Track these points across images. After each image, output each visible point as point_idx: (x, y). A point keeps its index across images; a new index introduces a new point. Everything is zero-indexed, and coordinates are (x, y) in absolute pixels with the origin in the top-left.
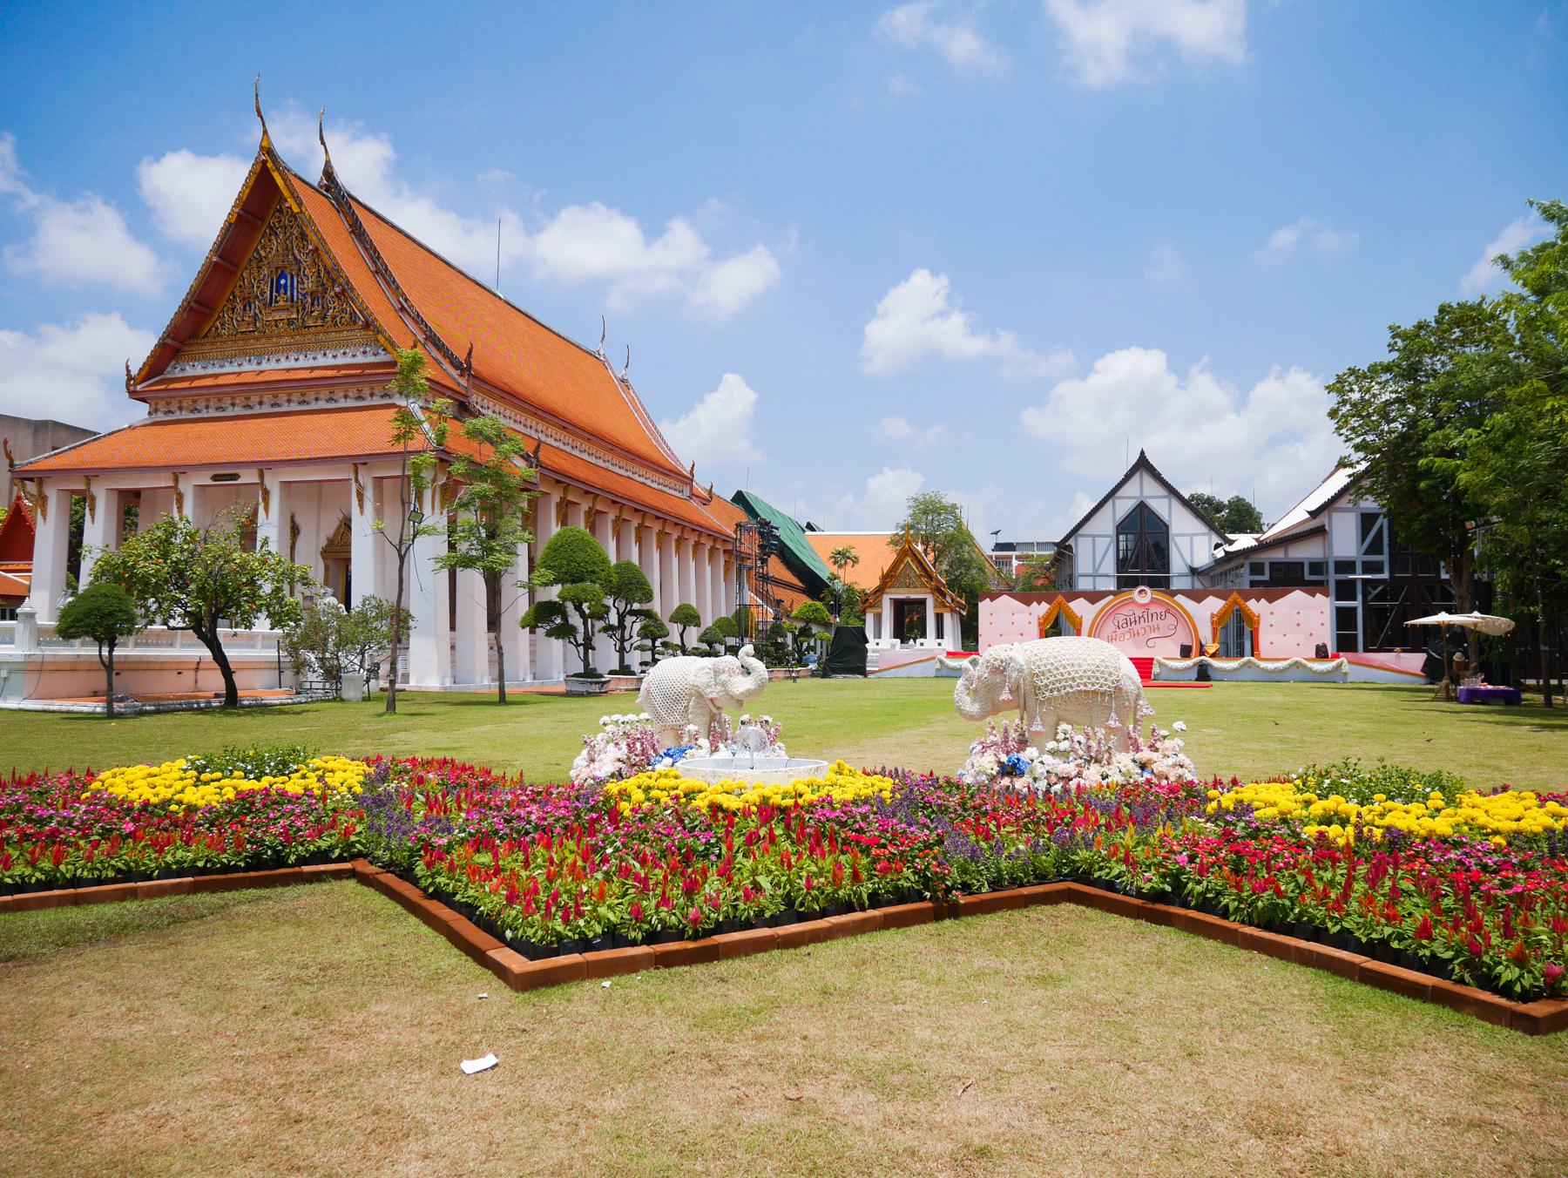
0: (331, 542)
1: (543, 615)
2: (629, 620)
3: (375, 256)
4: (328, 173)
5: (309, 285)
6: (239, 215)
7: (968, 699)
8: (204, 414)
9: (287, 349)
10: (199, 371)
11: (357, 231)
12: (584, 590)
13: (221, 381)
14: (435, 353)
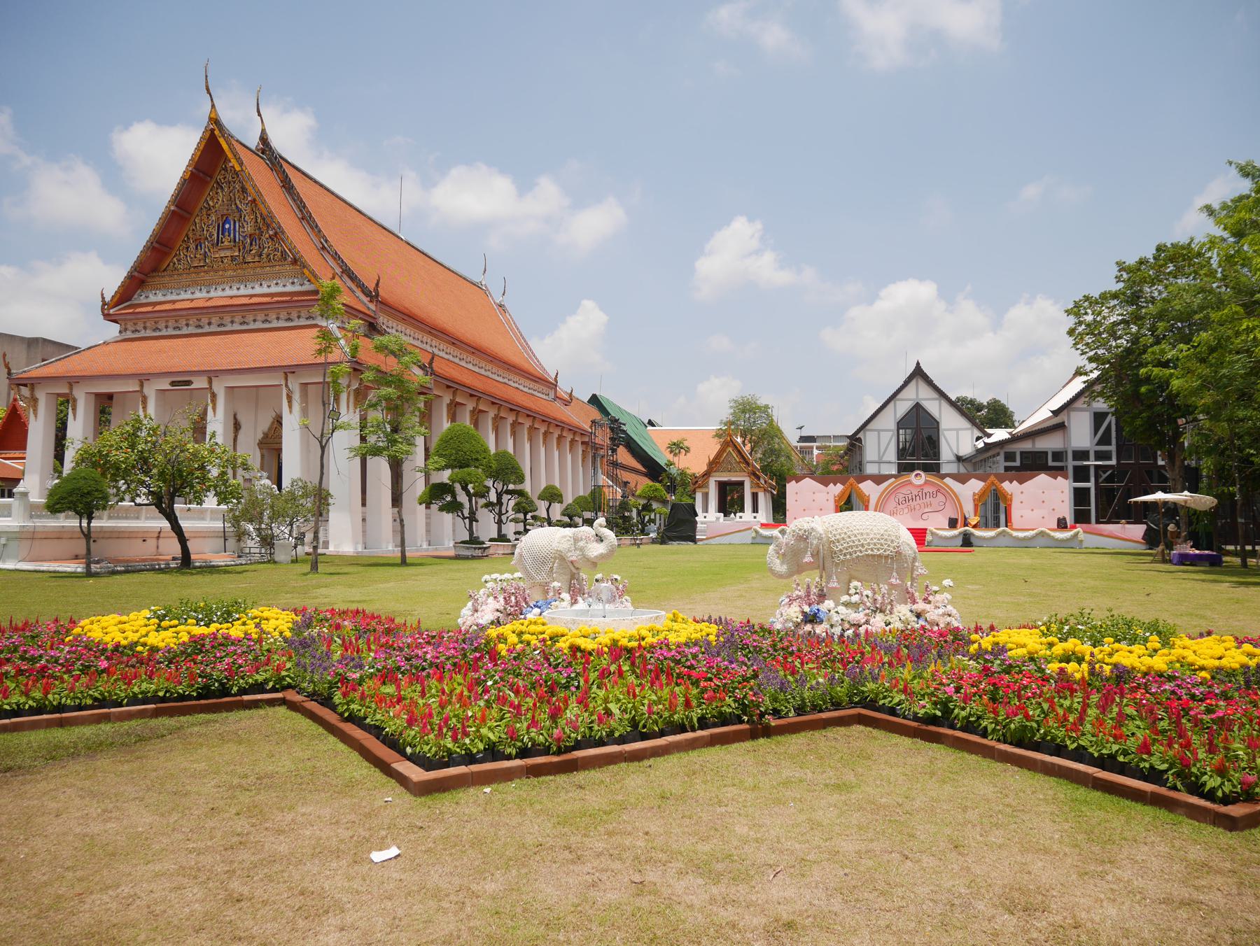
0: (266, 435)
1: (437, 494)
2: (505, 498)
3: (301, 206)
4: (264, 139)
5: (249, 229)
6: (192, 173)
7: (778, 561)
8: (164, 333)
9: (231, 281)
10: (160, 298)
11: (287, 185)
12: (469, 474)
13: (178, 306)
14: (349, 283)
